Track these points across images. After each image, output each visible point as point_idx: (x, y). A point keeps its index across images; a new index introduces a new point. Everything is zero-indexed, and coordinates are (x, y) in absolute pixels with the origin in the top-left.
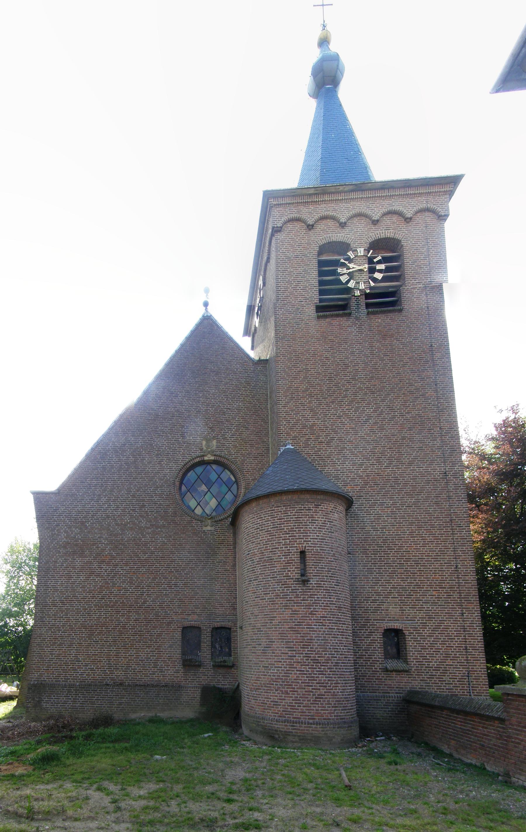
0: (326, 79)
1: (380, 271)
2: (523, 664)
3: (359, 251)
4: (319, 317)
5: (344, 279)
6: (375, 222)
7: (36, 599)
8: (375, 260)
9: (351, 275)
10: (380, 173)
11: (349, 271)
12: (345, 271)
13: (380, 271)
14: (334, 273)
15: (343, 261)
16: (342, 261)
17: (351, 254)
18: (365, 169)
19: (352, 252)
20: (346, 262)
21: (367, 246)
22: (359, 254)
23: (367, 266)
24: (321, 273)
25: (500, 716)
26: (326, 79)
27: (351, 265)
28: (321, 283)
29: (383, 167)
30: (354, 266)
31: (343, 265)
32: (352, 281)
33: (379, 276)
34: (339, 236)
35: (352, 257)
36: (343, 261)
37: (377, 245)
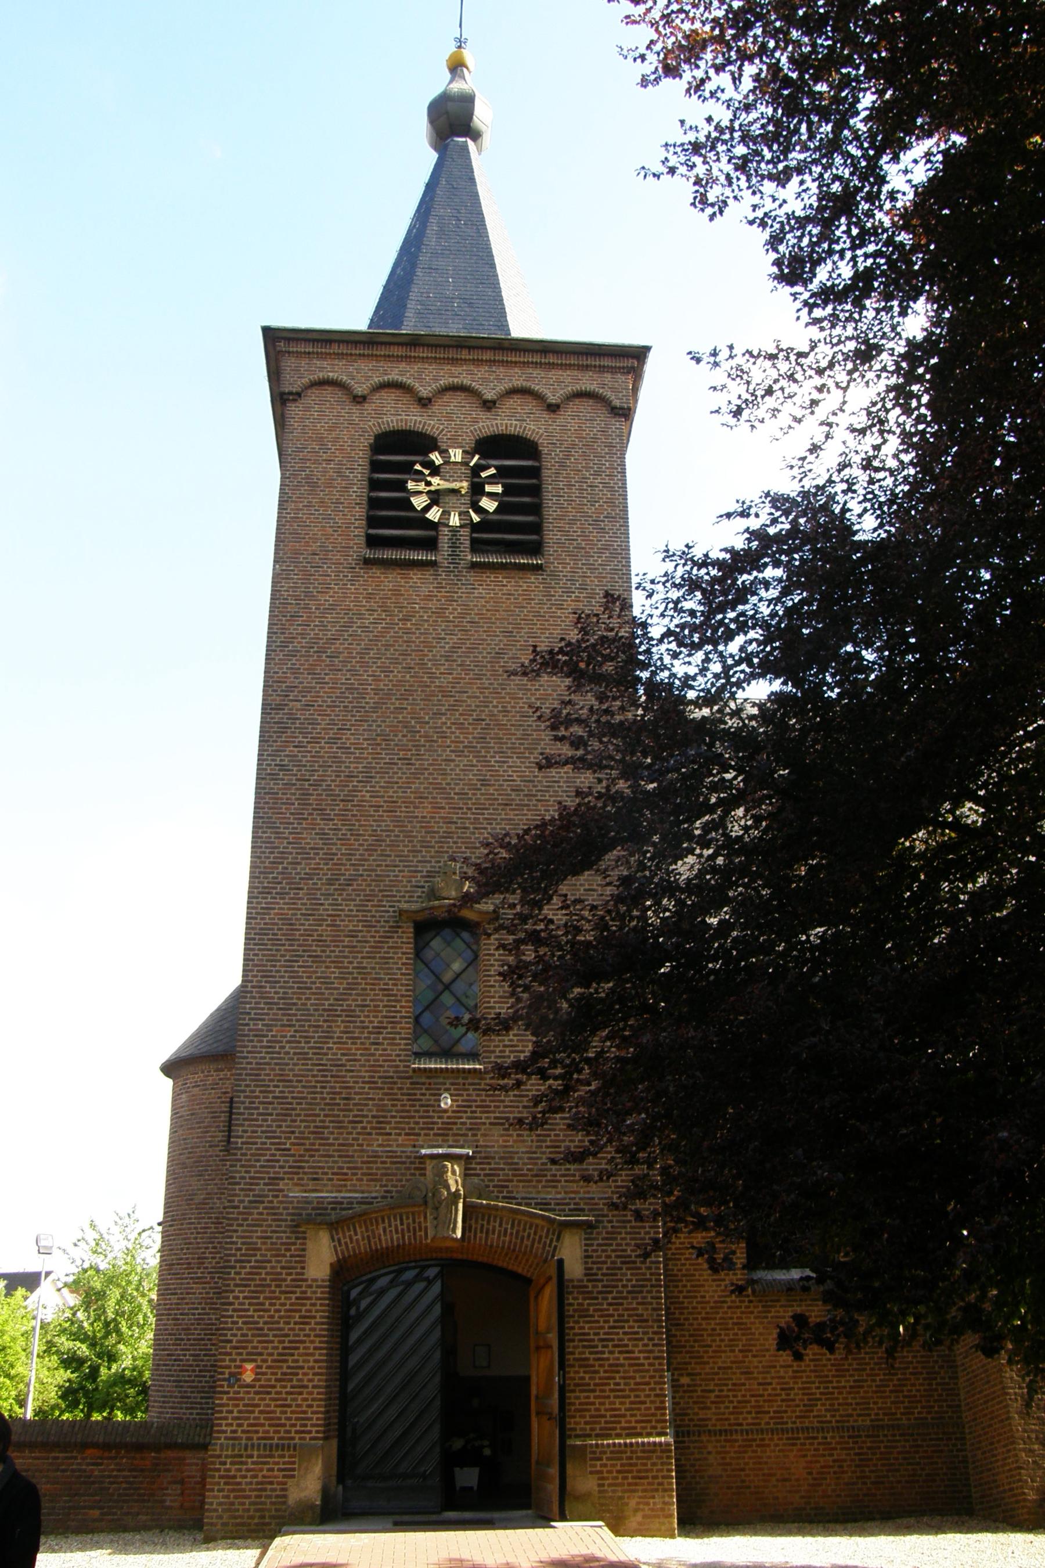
0: (452, 122)
1: (491, 495)
2: (504, 1009)
3: (452, 454)
4: (367, 562)
5: (419, 502)
6: (489, 405)
7: (596, 862)
8: (483, 475)
9: (436, 498)
10: (522, 325)
11: (428, 488)
12: (422, 486)
13: (491, 495)
14: (401, 486)
15: (424, 471)
16: (418, 467)
17: (436, 458)
18: (504, 326)
19: (440, 453)
20: (427, 472)
21: (469, 441)
22: (453, 459)
23: (465, 484)
24: (374, 485)
25: (150, 1301)
26: (452, 122)
27: (435, 481)
28: (374, 504)
29: (532, 314)
30: (441, 482)
31: (419, 477)
32: (435, 508)
33: (489, 505)
34: (413, 419)
35: (437, 463)
36: (424, 471)
37: (490, 446)
